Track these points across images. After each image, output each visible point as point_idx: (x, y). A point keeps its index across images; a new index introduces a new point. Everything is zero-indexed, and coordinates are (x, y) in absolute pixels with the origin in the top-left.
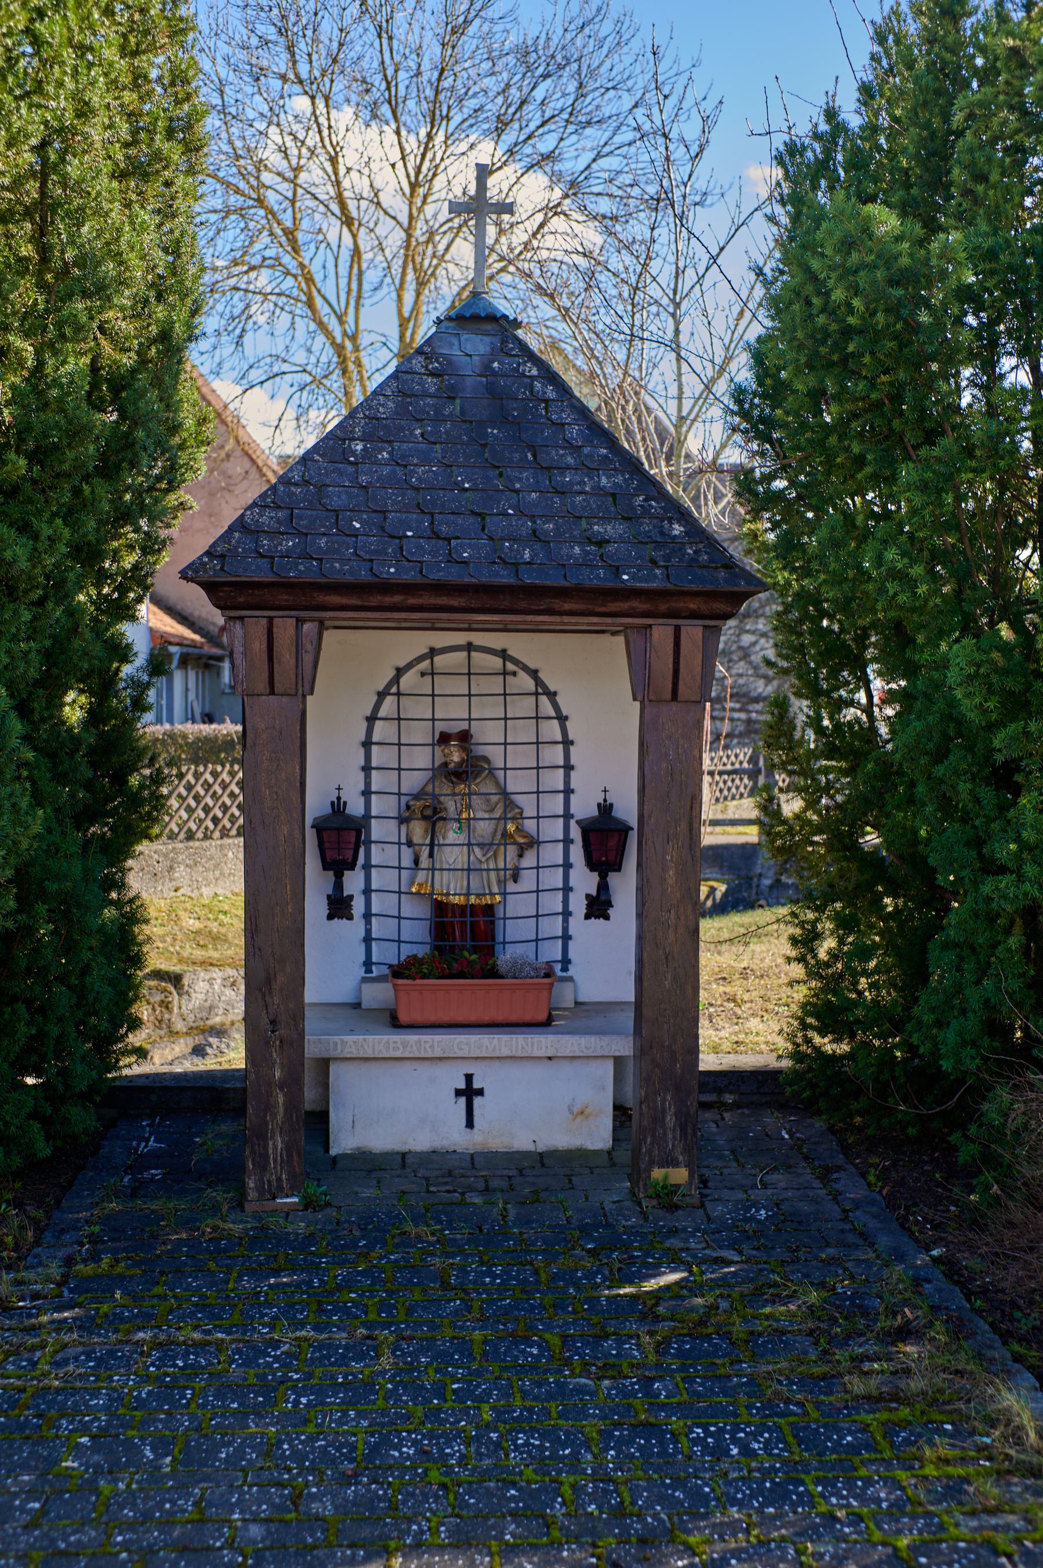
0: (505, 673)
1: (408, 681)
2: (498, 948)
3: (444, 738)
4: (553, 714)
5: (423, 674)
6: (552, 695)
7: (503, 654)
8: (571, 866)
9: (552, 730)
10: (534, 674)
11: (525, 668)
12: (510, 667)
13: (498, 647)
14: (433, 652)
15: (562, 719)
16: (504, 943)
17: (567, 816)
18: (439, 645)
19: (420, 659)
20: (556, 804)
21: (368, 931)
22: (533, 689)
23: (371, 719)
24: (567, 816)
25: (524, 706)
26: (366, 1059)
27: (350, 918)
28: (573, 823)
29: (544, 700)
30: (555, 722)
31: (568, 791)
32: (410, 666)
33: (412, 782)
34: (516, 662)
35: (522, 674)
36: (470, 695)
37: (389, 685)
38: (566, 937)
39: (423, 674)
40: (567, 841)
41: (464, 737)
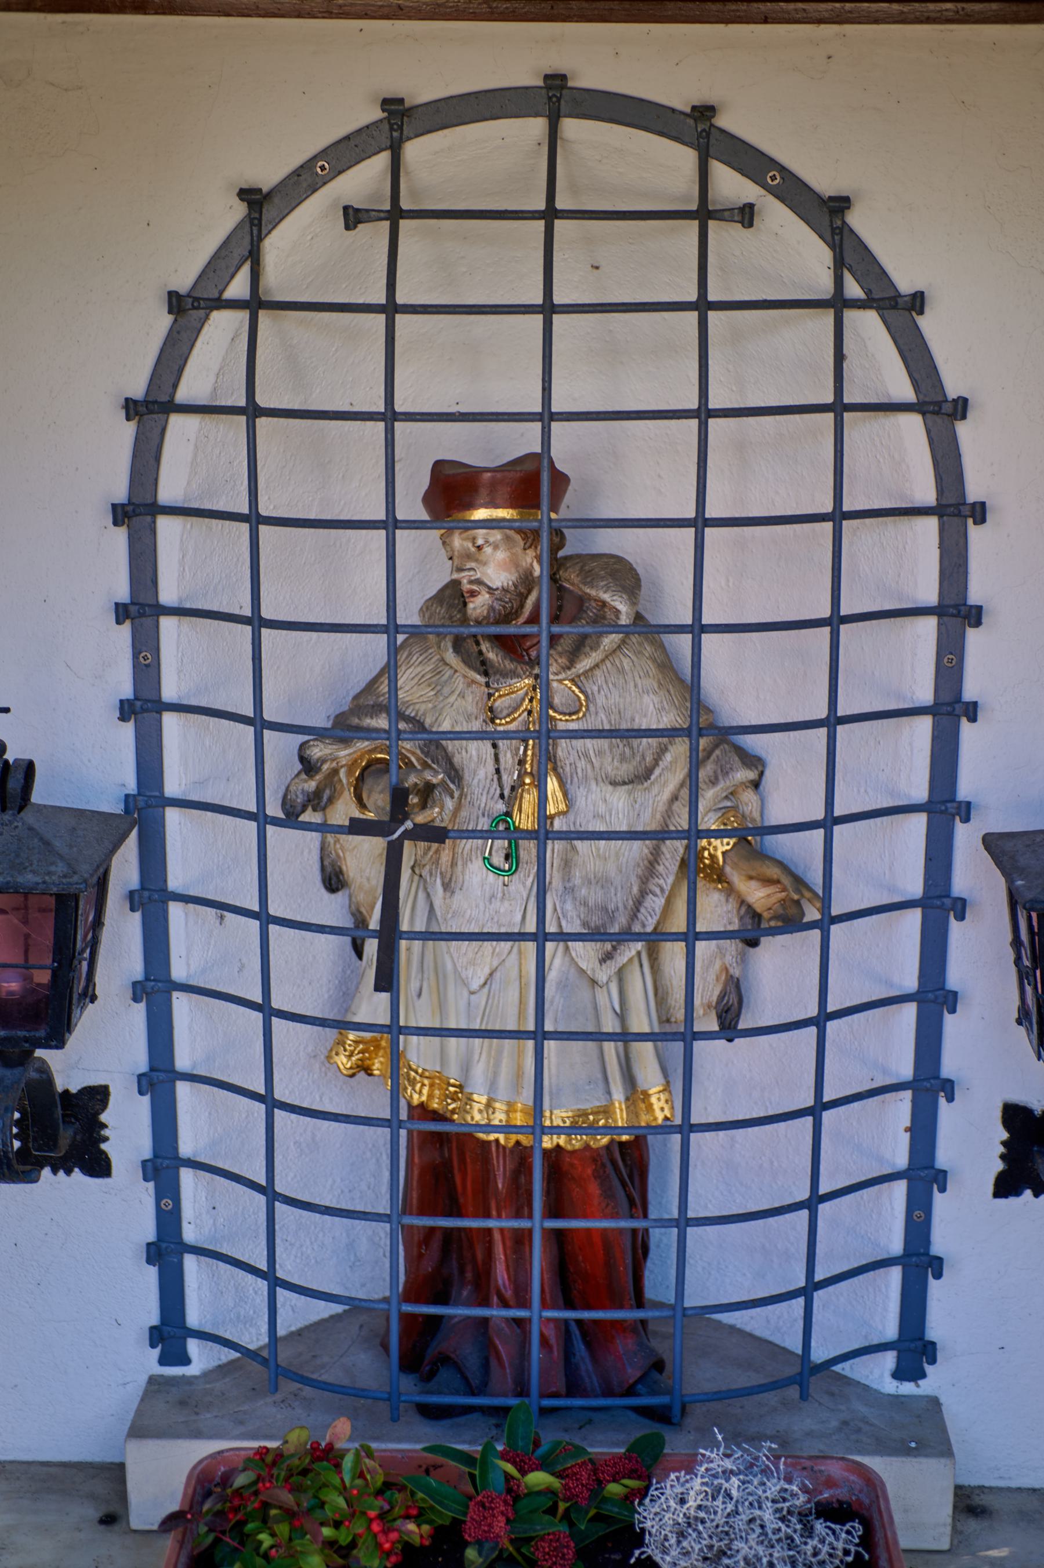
0: (704, 213)
1: (300, 248)
2: (663, 1242)
3: (452, 491)
4: (903, 390)
5: (353, 217)
6: (903, 309)
7: (700, 129)
8: (951, 1001)
9: (897, 457)
10: (829, 215)
11: (793, 191)
12: (730, 185)
13: (677, 93)
14: (400, 121)
15: (941, 411)
16: (683, 1222)
17: (944, 807)
18: (423, 89)
19: (345, 152)
20: (905, 758)
21: (169, 1220)
22: (823, 284)
23: (151, 410)
24: (944, 807)
25: (784, 358)
26: (839, 357)
27: (98, 1166)
28: (966, 838)
29: (868, 328)
30: (913, 425)
31: (951, 710)
32: (304, 181)
33: (311, 679)
34: (753, 162)
35: (777, 215)
36: (548, 309)
37: (218, 267)
38: (920, 1263)
39: (353, 217)
40: (940, 905)
41: (531, 484)
